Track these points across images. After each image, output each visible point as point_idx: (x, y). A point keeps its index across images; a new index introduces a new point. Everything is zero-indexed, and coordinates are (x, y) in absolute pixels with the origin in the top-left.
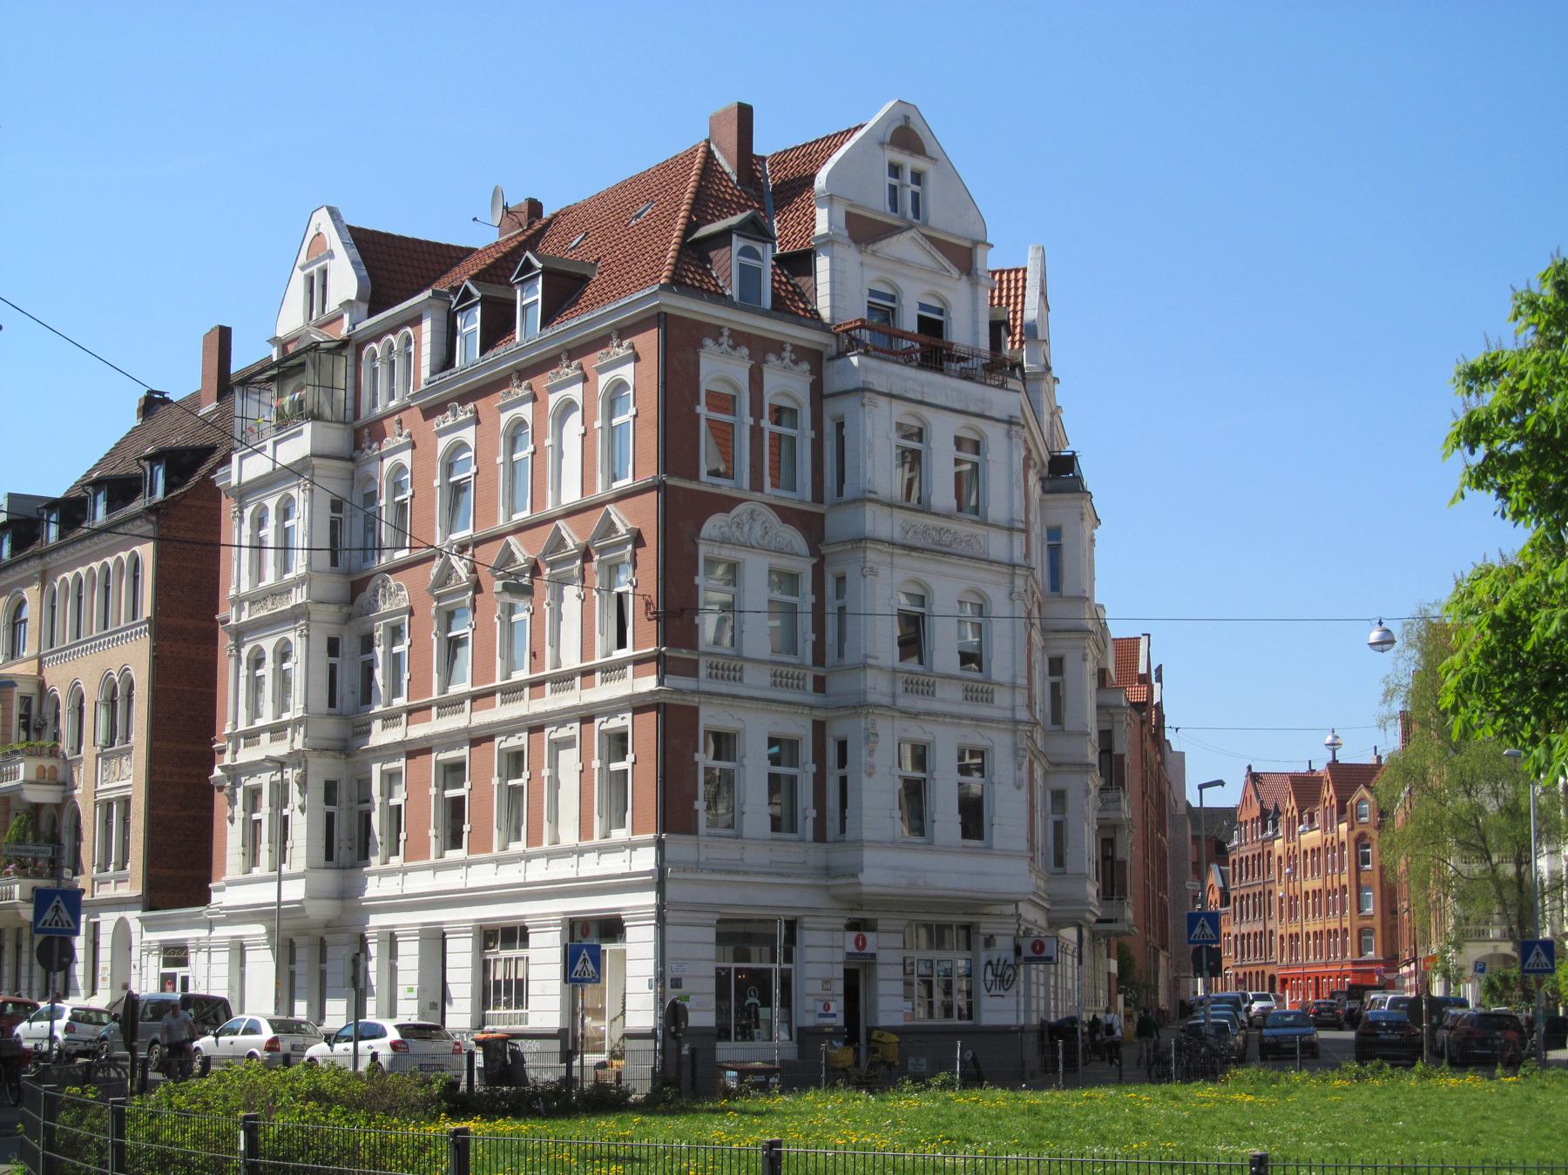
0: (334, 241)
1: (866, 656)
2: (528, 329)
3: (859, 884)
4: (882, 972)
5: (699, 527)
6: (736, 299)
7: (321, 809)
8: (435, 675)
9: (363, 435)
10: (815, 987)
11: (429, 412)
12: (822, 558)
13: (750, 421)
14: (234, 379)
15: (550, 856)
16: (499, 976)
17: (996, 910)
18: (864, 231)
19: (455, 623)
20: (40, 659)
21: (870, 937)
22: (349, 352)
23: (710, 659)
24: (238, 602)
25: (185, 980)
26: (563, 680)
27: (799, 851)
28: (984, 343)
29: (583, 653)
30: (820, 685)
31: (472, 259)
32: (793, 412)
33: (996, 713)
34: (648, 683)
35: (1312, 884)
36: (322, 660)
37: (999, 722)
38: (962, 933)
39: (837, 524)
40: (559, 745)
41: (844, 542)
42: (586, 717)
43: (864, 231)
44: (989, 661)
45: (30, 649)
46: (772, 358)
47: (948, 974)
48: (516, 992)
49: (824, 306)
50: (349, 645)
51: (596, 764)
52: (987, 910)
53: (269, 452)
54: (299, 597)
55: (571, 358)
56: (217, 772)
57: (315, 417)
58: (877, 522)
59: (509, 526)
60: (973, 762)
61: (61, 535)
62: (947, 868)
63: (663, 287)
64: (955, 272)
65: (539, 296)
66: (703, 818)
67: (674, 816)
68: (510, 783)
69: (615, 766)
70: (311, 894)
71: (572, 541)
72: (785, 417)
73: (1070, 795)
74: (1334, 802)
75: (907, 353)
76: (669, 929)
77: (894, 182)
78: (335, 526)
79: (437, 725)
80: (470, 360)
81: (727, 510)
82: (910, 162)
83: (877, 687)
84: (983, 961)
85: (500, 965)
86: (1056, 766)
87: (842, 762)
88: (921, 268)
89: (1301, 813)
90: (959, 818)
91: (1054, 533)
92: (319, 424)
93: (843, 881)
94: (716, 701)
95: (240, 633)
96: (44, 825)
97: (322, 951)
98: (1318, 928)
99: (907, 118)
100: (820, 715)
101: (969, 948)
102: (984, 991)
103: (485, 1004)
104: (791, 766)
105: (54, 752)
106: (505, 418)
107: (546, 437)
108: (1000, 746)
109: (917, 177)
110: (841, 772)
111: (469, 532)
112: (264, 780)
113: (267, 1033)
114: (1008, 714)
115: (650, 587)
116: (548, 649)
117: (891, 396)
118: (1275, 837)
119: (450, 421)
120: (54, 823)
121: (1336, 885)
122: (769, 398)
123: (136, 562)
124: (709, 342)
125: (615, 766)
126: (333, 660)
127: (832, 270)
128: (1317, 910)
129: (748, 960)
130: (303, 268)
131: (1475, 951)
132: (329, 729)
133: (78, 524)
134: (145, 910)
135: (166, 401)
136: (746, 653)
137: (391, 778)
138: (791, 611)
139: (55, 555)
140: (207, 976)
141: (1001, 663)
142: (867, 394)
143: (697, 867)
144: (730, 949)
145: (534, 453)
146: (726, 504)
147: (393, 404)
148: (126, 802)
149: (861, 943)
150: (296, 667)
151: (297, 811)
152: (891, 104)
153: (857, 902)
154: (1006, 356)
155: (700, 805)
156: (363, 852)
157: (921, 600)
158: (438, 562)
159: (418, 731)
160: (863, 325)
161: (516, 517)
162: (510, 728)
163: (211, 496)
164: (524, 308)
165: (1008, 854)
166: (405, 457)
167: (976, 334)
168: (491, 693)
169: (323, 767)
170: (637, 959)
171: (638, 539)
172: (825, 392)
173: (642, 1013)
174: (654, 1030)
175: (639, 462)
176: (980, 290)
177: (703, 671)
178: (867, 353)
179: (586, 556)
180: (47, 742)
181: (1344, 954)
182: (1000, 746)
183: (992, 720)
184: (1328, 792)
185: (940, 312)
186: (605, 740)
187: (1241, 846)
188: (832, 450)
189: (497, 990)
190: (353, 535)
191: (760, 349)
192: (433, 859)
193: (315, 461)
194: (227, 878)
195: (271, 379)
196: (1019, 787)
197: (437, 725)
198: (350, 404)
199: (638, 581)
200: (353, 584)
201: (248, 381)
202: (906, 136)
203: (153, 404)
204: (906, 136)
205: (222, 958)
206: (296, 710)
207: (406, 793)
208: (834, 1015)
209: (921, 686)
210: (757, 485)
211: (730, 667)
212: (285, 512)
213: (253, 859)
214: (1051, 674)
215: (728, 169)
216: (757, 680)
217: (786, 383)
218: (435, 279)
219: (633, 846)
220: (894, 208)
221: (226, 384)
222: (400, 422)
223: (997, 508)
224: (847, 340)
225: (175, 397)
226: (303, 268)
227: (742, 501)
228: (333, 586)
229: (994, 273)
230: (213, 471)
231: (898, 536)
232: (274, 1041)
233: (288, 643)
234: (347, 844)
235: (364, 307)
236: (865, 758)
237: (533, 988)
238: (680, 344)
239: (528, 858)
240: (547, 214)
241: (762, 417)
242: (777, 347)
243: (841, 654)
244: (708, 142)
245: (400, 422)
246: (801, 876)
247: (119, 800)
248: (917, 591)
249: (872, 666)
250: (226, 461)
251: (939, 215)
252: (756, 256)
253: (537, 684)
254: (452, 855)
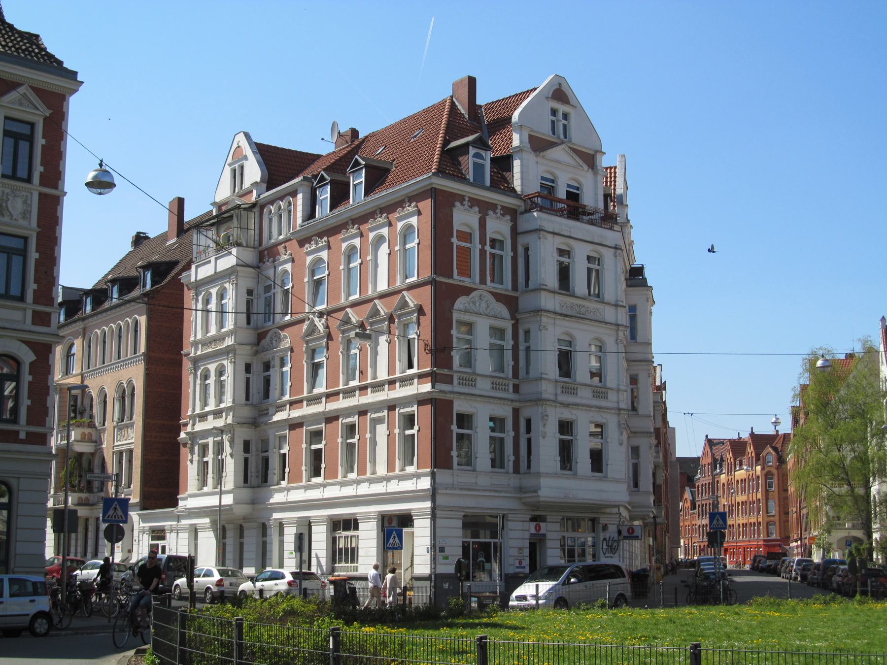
0: (248, 151)
1: (541, 374)
2: (357, 197)
3: (538, 496)
4: (549, 544)
5: (453, 305)
6: (471, 180)
7: (242, 455)
8: (305, 384)
9: (265, 255)
10: (514, 552)
11: (302, 243)
12: (517, 321)
13: (480, 247)
14: (186, 227)
15: (371, 481)
16: (342, 546)
17: (608, 510)
18: (538, 145)
19: (316, 356)
20: (82, 375)
21: (542, 525)
22: (257, 210)
23: (459, 374)
24: (195, 344)
25: (164, 548)
26: (378, 386)
27: (506, 479)
28: (601, 205)
29: (392, 371)
30: (516, 389)
31: (320, 160)
32: (502, 242)
33: (610, 405)
34: (426, 387)
35: (741, 498)
36: (243, 375)
37: (611, 409)
38: (590, 523)
39: (526, 302)
40: (376, 422)
41: (529, 312)
42: (391, 407)
43: (538, 145)
44: (605, 377)
45: (76, 370)
46: (491, 213)
47: (583, 544)
48: (351, 554)
49: (517, 184)
50: (257, 367)
51: (397, 431)
52: (603, 511)
53: (211, 265)
54: (229, 342)
55: (410, 202)
56: (183, 435)
57: (238, 245)
58: (548, 301)
59: (347, 303)
60: (600, 430)
61: (93, 309)
62: (582, 488)
63: (434, 174)
64: (586, 167)
65: (363, 179)
66: (455, 460)
67: (440, 460)
68: (349, 441)
69: (408, 432)
70: (236, 501)
71: (383, 311)
72: (497, 245)
73: (641, 449)
74: (753, 454)
75: (562, 210)
76: (438, 520)
77: (554, 118)
78: (249, 303)
79: (306, 410)
80: (324, 214)
81: (468, 295)
82: (562, 108)
83: (547, 390)
84: (602, 538)
85: (342, 540)
86: (634, 434)
87: (529, 430)
88: (568, 165)
89: (735, 460)
90: (590, 461)
91: (633, 309)
92: (241, 248)
93: (530, 495)
94: (462, 397)
95: (196, 361)
96: (85, 464)
97: (243, 533)
98: (745, 521)
99: (560, 84)
100: (517, 405)
101: (594, 531)
102: (602, 554)
103: (334, 561)
104: (501, 432)
105: (92, 425)
106: (344, 245)
107: (368, 255)
108: (612, 423)
109: (566, 116)
110: (528, 436)
111: (324, 306)
112: (210, 441)
113: (217, 577)
114: (615, 405)
115: (427, 335)
116: (369, 369)
117: (554, 233)
118: (721, 473)
119: (314, 247)
120: (90, 463)
121: (754, 499)
122: (489, 235)
123: (136, 323)
124: (458, 204)
125: (408, 432)
126: (248, 375)
127: (522, 165)
128: (744, 512)
129: (479, 538)
130: (230, 165)
131: (838, 535)
132: (246, 412)
133: (76, 313)
134: (141, 510)
135: (147, 238)
136: (478, 371)
137: (283, 438)
138: (501, 349)
139: (91, 319)
140: (177, 545)
141: (611, 379)
142: (542, 233)
143: (453, 487)
144: (469, 532)
145: (361, 264)
146: (467, 291)
147: (281, 237)
148: (131, 452)
149: (538, 528)
150: (228, 378)
151: (229, 456)
152: (552, 77)
153: (536, 506)
154: (611, 215)
155: (454, 453)
156: (265, 479)
157: (570, 343)
158: (307, 323)
159: (296, 413)
160: (539, 195)
161: (351, 298)
162: (348, 412)
163: (178, 288)
164: (355, 186)
165: (616, 481)
166: (288, 267)
167: (596, 201)
168: (337, 394)
169: (243, 433)
170: (421, 534)
171: (420, 311)
172: (519, 231)
173: (422, 566)
174: (430, 575)
175: (419, 269)
176: (599, 178)
177: (455, 381)
178: (541, 211)
179: (391, 319)
180: (86, 420)
181: (759, 535)
182: (612, 423)
183: (607, 408)
184: (750, 449)
185: (578, 189)
186: (402, 418)
187: (702, 478)
188: (524, 261)
189: (342, 554)
190: (259, 306)
191: (485, 208)
192: (304, 483)
193: (239, 268)
194: (188, 492)
195: (212, 225)
196: (621, 445)
197: (306, 410)
198: (257, 238)
199: (419, 333)
200: (259, 334)
201: (199, 225)
202: (559, 93)
203: (140, 239)
204: (559, 93)
205: (184, 536)
206: (228, 402)
207: (294, 448)
208: (524, 567)
209: (571, 390)
210: (483, 281)
211: (470, 380)
212: (221, 296)
213: (203, 482)
214: (631, 384)
215: (463, 112)
216: (483, 386)
217: (498, 226)
218: (305, 168)
219: (418, 476)
220: (554, 133)
221: (182, 228)
222: (285, 248)
223: (609, 294)
224: (530, 203)
225: (152, 235)
226: (230, 165)
227: (476, 289)
228: (248, 335)
229: (607, 168)
230: (179, 273)
231: (558, 310)
232: (221, 580)
233: (223, 366)
234: (258, 472)
235: (264, 186)
236: (541, 428)
237: (361, 552)
238: (443, 205)
239: (358, 482)
240: (361, 136)
241: (485, 244)
242: (493, 207)
243: (527, 372)
244: (452, 97)
245: (285, 248)
246: (507, 492)
247: (126, 450)
248: (567, 338)
249: (545, 379)
250: (187, 267)
251: (577, 137)
252: (482, 158)
253: (392, 383)
254: (315, 480)
